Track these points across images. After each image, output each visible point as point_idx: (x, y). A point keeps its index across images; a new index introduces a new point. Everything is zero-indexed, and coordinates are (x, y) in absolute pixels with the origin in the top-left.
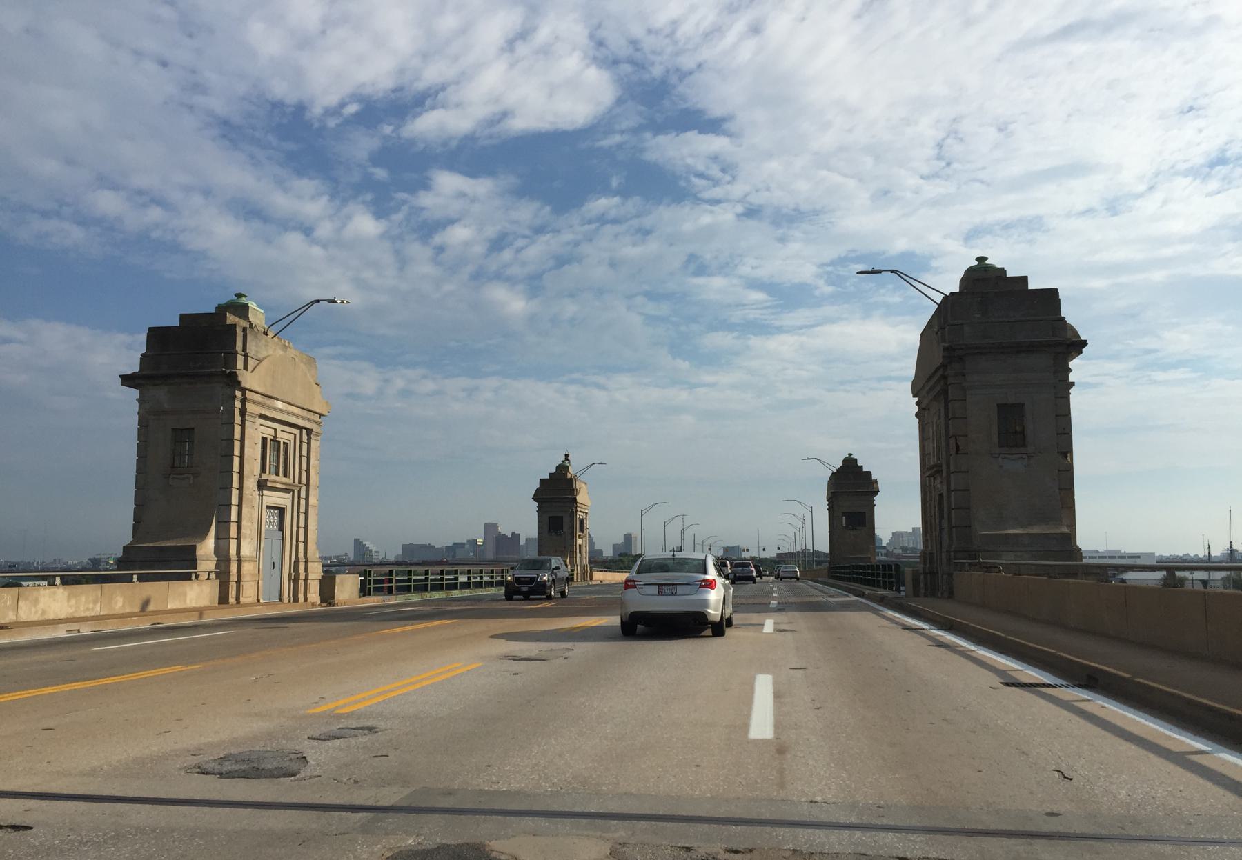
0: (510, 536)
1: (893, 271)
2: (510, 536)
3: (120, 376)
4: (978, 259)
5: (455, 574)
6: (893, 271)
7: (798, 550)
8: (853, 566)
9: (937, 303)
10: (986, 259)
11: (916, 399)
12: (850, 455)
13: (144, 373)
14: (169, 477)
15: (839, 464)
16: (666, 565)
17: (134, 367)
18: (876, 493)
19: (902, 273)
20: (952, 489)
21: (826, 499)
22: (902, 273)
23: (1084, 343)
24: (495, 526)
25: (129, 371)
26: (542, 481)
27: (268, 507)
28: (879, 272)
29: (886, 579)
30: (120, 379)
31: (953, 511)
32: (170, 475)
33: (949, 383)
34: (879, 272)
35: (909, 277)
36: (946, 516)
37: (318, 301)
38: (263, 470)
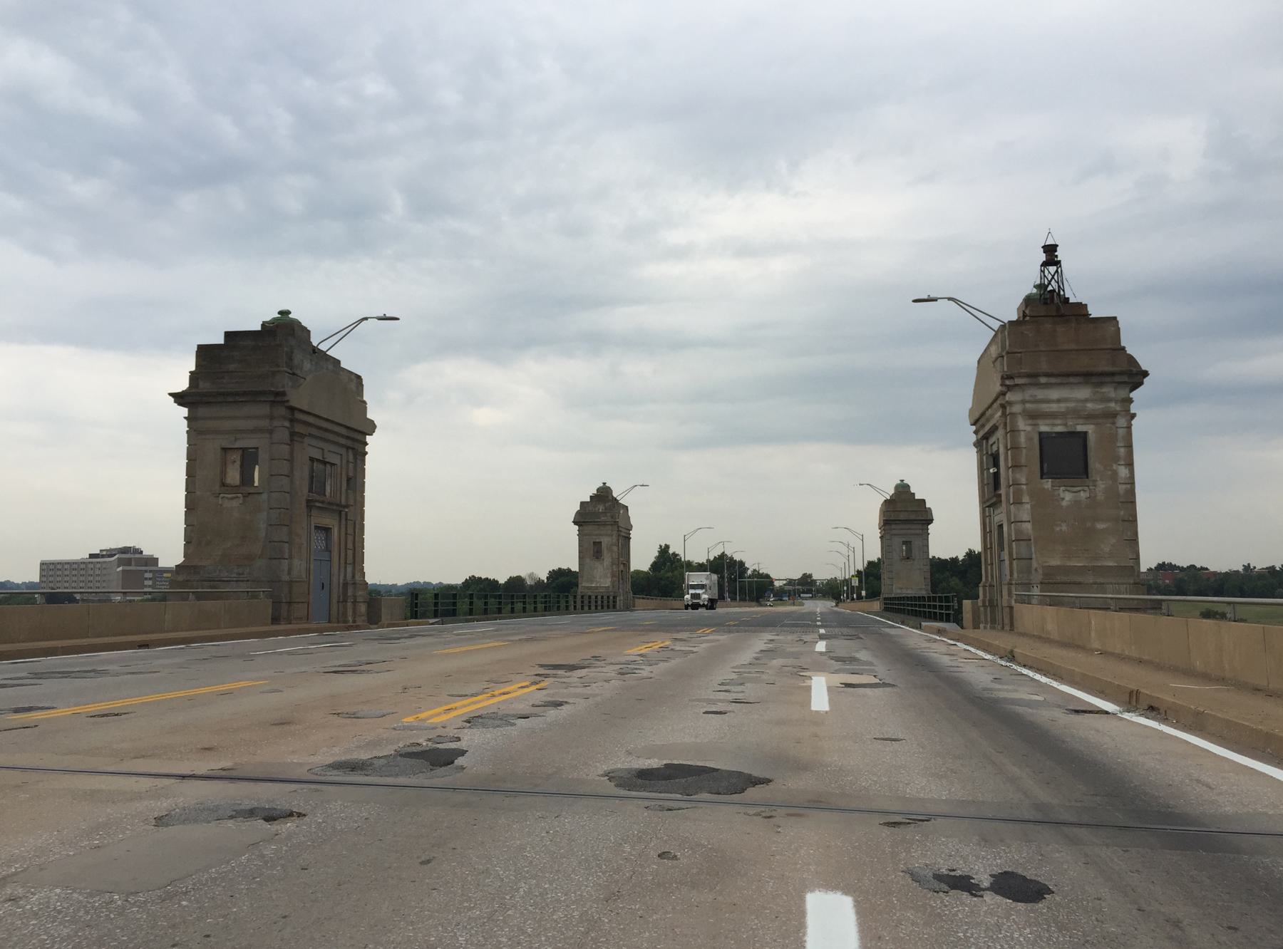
0: (876, 561)
1: (950, 299)
2: (876, 561)
3: (171, 394)
4: (280, 313)
5: (499, 599)
6: (950, 299)
7: (847, 578)
8: (908, 597)
9: (994, 330)
10: (289, 312)
11: (974, 428)
12: (604, 484)
13: (194, 390)
14: (218, 497)
15: (892, 492)
16: (380, 592)
17: (183, 385)
18: (931, 521)
19: (961, 302)
20: (1013, 520)
21: (877, 527)
22: (961, 302)
23: (1145, 374)
24: (667, 547)
25: (179, 390)
26: (582, 504)
27: (316, 527)
28: (935, 300)
29: (937, 611)
30: (1144, 368)
31: (1014, 543)
32: (220, 494)
33: (1007, 413)
34: (935, 300)
35: (971, 307)
36: (1006, 546)
37: (366, 319)
38: (310, 490)
